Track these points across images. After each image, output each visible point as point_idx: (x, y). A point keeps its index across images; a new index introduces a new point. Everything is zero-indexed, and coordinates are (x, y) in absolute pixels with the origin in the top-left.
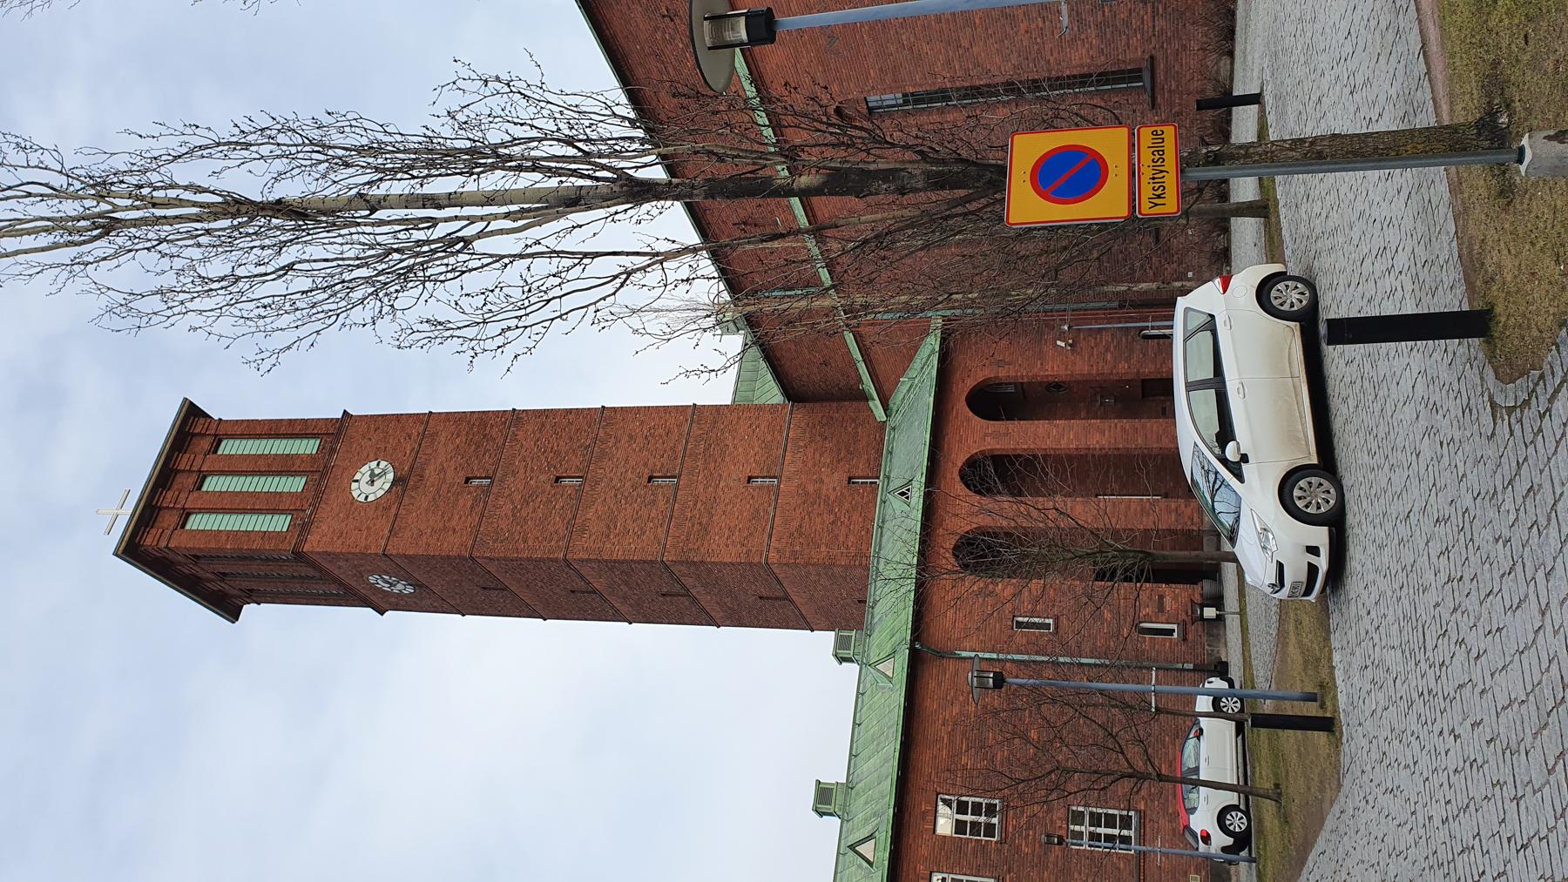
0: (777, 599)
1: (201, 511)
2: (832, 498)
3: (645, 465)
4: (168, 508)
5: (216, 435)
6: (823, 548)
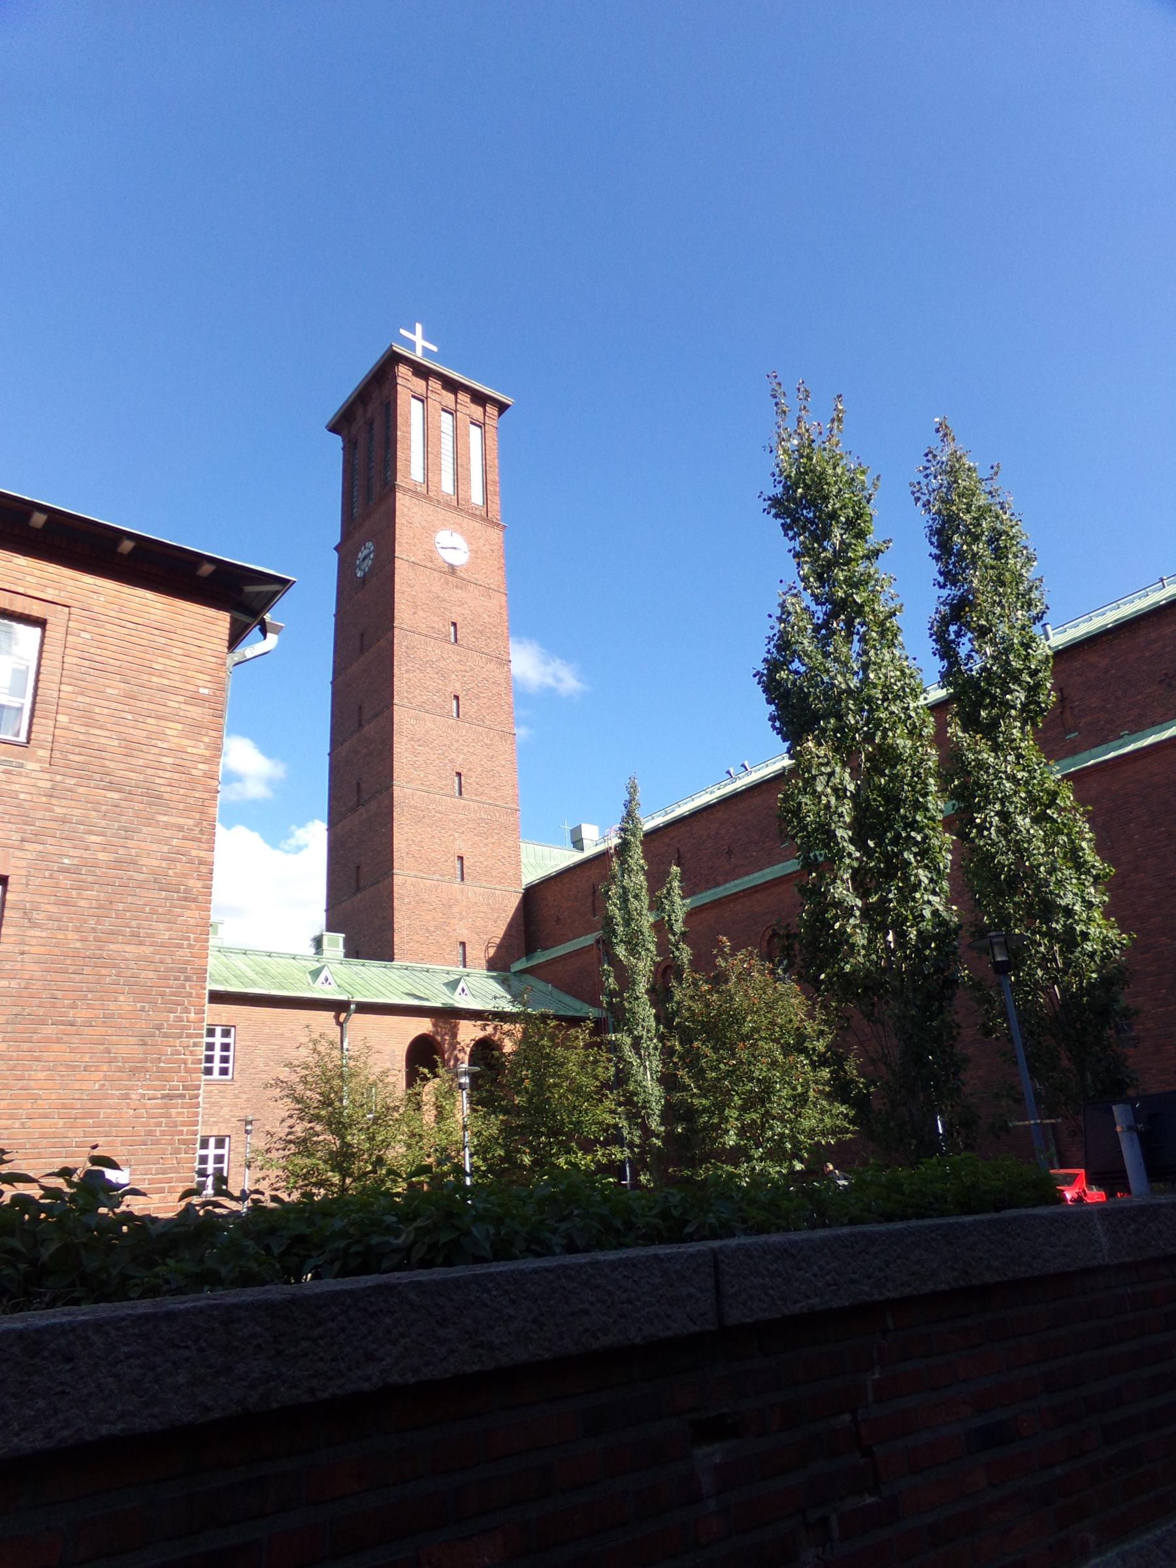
0: (358, 881)
1: (455, 428)
2: (447, 928)
3: (470, 770)
4: (427, 385)
5: (484, 424)
6: (407, 922)
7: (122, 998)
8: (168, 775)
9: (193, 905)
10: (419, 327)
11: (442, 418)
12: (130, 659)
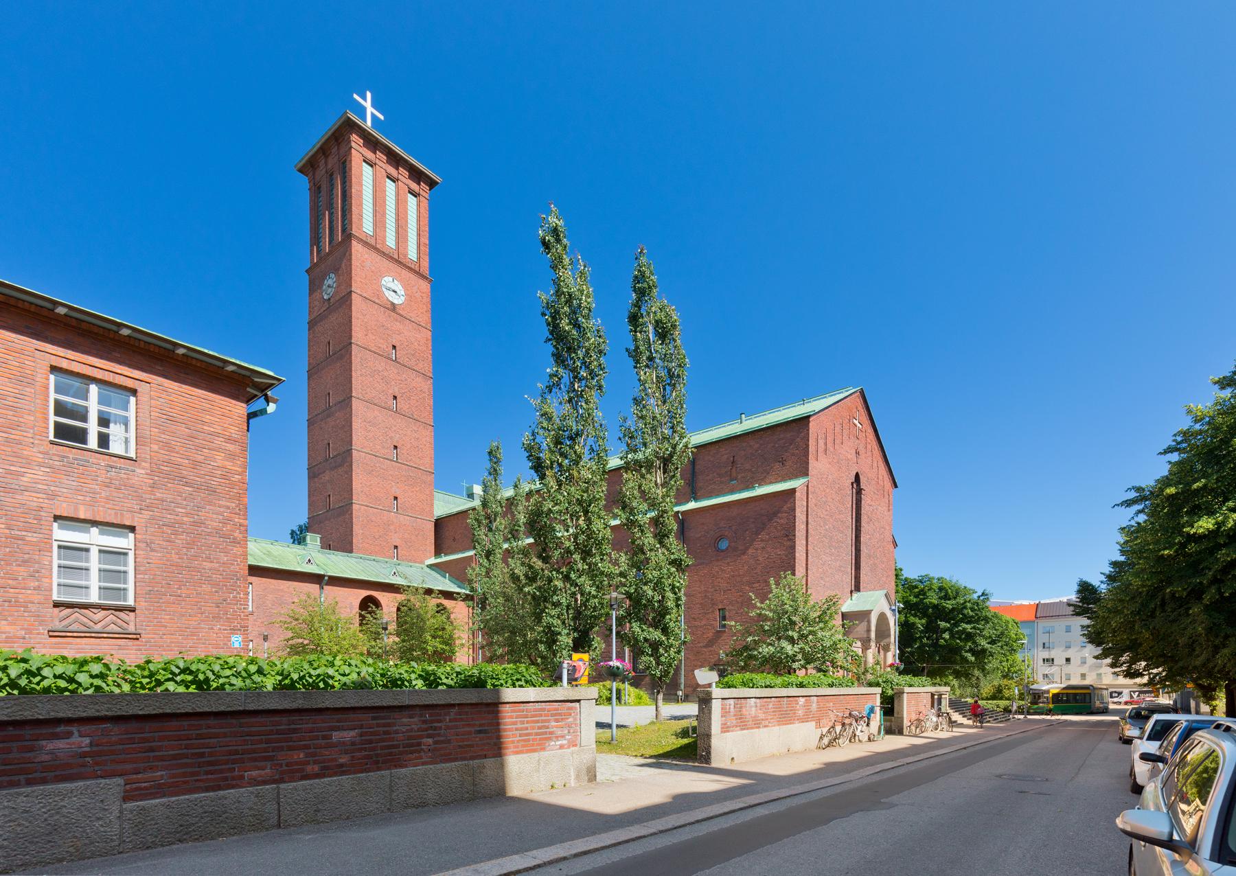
3: (403, 445)
7: (204, 586)
8: (218, 480)
9: (238, 545)
10: (369, 95)
12: (189, 415)
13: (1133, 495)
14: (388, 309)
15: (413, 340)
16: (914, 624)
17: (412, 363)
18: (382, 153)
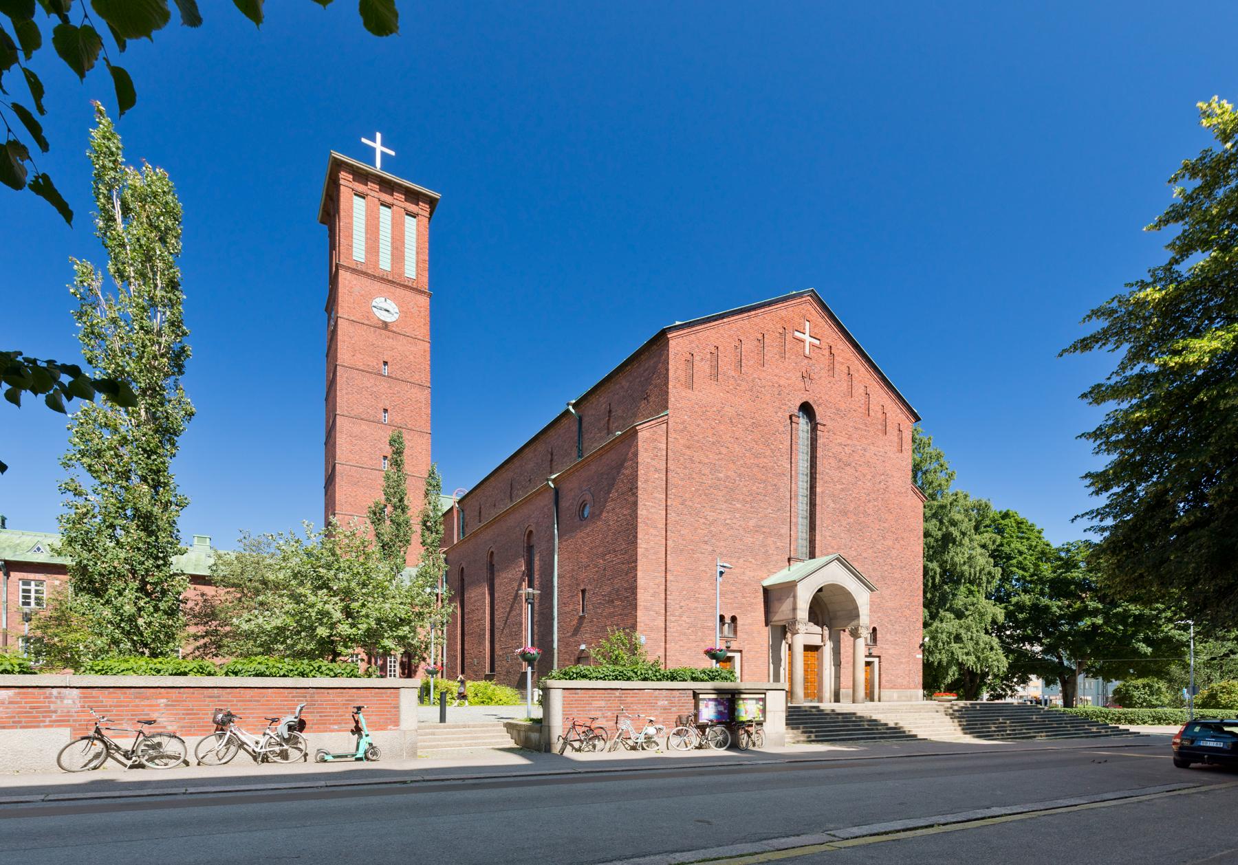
10: (378, 136)
11: (381, 211)
13: (1100, 324)
14: (379, 328)
15: (408, 354)
16: (1047, 608)
17: (407, 376)
18: (374, 183)
